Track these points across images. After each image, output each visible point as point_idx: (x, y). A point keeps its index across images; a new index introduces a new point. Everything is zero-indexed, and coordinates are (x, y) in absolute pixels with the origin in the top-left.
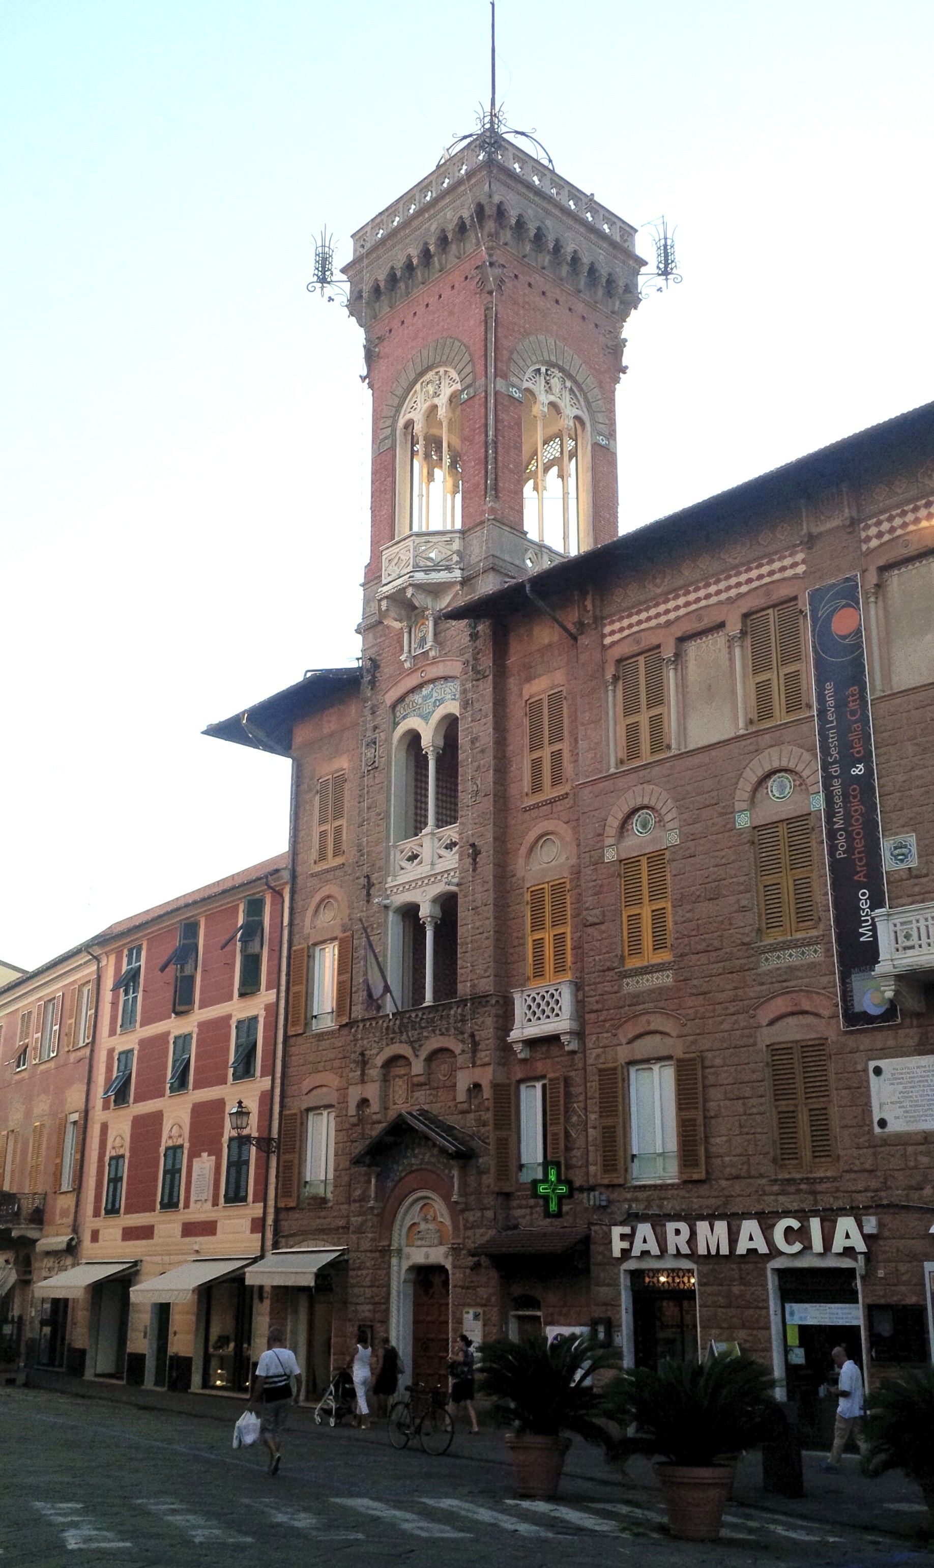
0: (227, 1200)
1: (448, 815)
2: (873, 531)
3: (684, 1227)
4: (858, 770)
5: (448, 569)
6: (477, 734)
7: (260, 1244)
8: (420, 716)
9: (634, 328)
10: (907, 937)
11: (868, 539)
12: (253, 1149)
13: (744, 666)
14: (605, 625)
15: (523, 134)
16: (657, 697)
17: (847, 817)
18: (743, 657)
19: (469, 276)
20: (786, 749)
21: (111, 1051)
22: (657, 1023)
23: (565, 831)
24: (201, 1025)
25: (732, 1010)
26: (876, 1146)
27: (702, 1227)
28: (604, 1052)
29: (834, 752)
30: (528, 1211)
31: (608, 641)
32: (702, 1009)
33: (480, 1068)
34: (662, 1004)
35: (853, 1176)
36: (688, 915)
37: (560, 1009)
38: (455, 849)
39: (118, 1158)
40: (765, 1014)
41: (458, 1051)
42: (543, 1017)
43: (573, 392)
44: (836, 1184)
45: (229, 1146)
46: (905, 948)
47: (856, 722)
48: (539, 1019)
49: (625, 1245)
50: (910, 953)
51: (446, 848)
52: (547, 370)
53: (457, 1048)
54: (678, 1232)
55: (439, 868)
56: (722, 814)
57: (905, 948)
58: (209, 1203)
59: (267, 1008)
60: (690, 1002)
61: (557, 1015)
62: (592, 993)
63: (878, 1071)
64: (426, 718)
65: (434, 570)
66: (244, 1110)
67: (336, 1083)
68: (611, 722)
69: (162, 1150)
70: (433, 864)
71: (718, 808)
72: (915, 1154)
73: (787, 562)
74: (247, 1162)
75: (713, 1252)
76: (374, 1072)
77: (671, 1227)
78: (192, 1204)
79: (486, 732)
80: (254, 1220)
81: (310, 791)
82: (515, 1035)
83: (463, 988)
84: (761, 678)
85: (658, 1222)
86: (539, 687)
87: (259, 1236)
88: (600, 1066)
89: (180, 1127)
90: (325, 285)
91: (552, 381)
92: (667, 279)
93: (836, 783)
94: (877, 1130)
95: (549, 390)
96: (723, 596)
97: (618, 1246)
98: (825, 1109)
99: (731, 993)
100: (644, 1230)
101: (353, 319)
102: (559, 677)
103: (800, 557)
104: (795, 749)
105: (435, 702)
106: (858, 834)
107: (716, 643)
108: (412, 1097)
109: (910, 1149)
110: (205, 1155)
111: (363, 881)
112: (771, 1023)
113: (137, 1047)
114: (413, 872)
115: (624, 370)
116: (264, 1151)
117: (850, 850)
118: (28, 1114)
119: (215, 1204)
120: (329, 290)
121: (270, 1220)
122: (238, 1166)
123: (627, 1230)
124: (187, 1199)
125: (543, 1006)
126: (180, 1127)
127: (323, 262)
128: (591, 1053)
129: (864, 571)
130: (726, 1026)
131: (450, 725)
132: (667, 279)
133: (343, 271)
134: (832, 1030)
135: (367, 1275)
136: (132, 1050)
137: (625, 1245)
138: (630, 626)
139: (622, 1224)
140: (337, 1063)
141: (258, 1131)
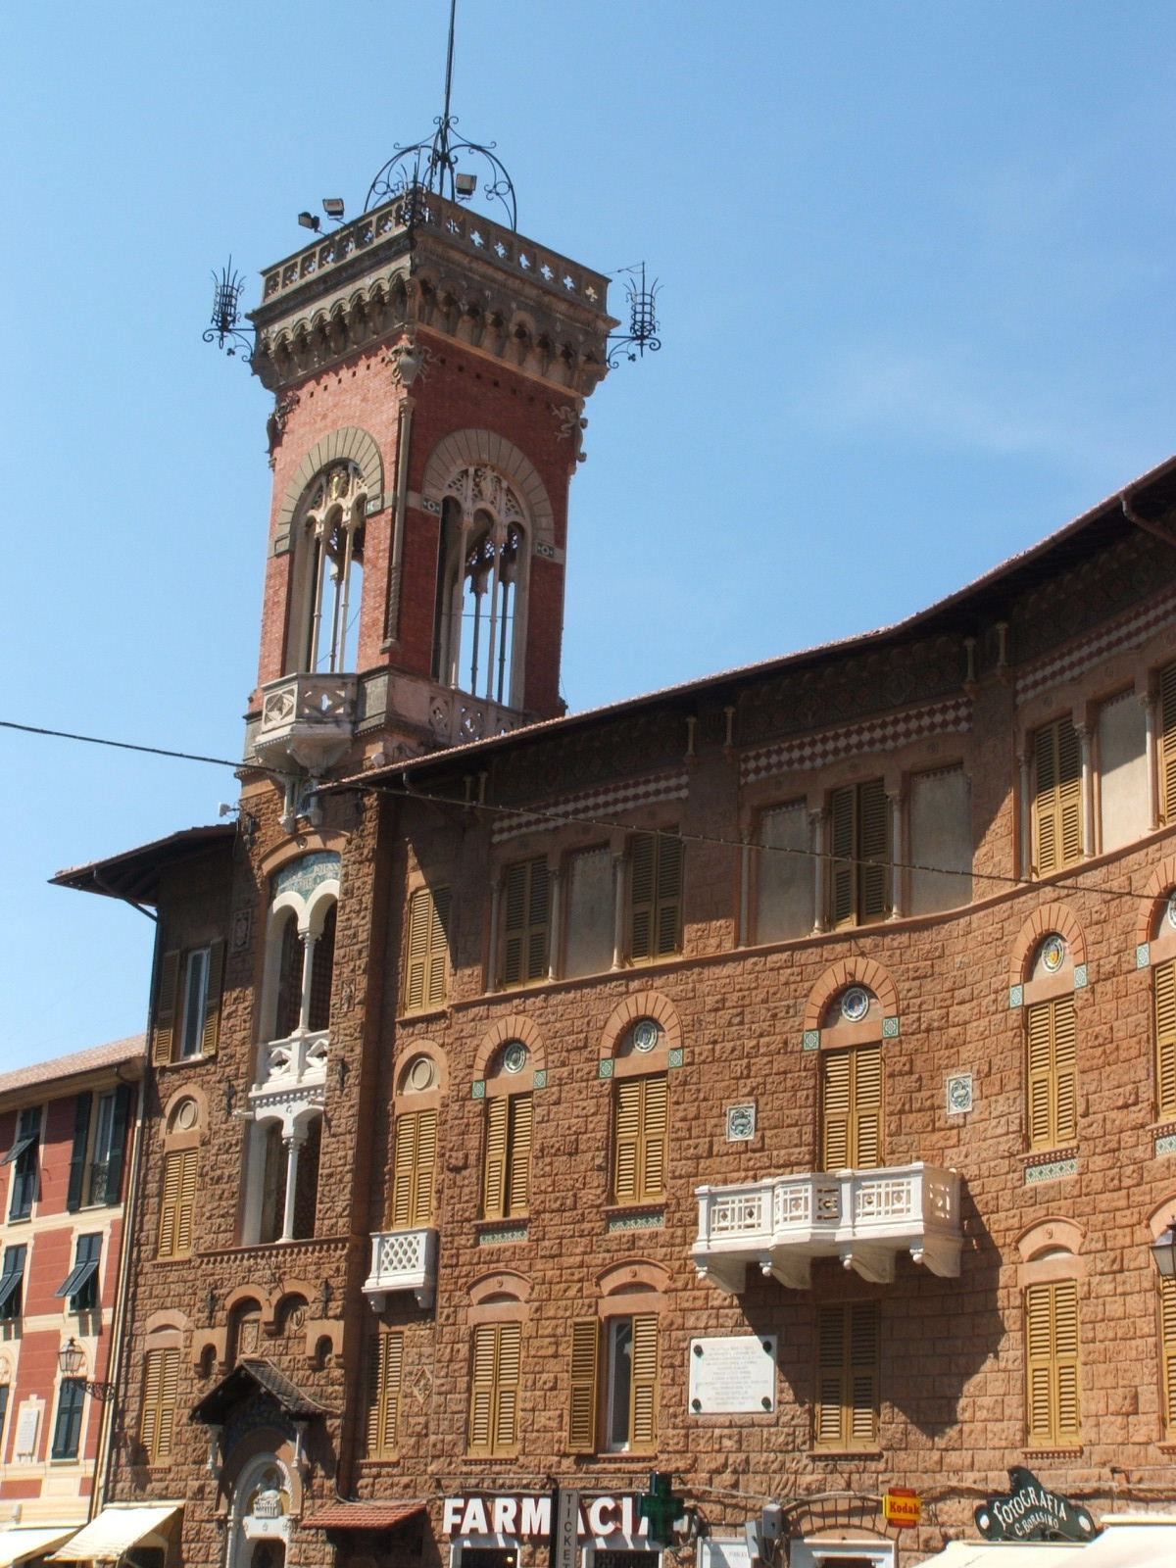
0: (56, 1455)
1: (318, 1021)
2: (752, 765)
3: (511, 1503)
6: (356, 928)
7: (88, 1510)
8: (299, 891)
11: (747, 773)
12: (88, 1398)
13: (625, 893)
14: (494, 820)
15: (479, 148)
16: (541, 916)
18: (625, 882)
19: (387, 359)
20: (652, 994)
22: (510, 1285)
23: (439, 1054)
24: (38, 1237)
27: (528, 1504)
28: (455, 1312)
30: (371, 1480)
33: (332, 1321)
36: (548, 1168)
37: (417, 1259)
38: (326, 1059)
40: (610, 1282)
41: (310, 1299)
42: (399, 1267)
43: (513, 494)
45: (61, 1389)
48: (395, 1268)
49: (457, 1519)
50: (725, 1234)
51: (318, 1056)
52: (476, 471)
53: (311, 1294)
54: (505, 1509)
56: (588, 1060)
58: (35, 1458)
59: (113, 1224)
60: (539, 1265)
61: (414, 1266)
62: (449, 1245)
63: (699, 1351)
66: (77, 1349)
67: (184, 1323)
68: (493, 936)
71: (585, 1054)
72: (721, 1437)
73: (673, 782)
74: (80, 1410)
75: (535, 1532)
77: (500, 1503)
78: (15, 1458)
79: (363, 925)
80: (84, 1480)
82: (371, 1285)
84: (641, 908)
85: (487, 1498)
87: (87, 1499)
89: (7, 1361)
90: (225, 334)
91: (483, 484)
92: (642, 345)
94: (692, 1410)
95: (478, 494)
96: (611, 810)
97: (449, 1520)
98: (838, 1380)
99: (578, 1259)
100: (475, 1505)
101: (257, 378)
103: (684, 779)
105: (315, 879)
107: (601, 861)
108: (261, 1346)
109: (717, 1432)
110: (33, 1397)
113: (31, 1244)
115: (583, 458)
116: (99, 1399)
119: (42, 1458)
120: (230, 340)
121: (101, 1482)
122: (70, 1413)
123: (460, 1503)
125: (401, 1255)
126: (7, 1361)
127: (226, 300)
128: (441, 1313)
131: (328, 911)
132: (642, 345)
133: (248, 317)
135: (200, 1549)
137: (457, 1519)
139: (456, 1496)
141: (96, 1372)
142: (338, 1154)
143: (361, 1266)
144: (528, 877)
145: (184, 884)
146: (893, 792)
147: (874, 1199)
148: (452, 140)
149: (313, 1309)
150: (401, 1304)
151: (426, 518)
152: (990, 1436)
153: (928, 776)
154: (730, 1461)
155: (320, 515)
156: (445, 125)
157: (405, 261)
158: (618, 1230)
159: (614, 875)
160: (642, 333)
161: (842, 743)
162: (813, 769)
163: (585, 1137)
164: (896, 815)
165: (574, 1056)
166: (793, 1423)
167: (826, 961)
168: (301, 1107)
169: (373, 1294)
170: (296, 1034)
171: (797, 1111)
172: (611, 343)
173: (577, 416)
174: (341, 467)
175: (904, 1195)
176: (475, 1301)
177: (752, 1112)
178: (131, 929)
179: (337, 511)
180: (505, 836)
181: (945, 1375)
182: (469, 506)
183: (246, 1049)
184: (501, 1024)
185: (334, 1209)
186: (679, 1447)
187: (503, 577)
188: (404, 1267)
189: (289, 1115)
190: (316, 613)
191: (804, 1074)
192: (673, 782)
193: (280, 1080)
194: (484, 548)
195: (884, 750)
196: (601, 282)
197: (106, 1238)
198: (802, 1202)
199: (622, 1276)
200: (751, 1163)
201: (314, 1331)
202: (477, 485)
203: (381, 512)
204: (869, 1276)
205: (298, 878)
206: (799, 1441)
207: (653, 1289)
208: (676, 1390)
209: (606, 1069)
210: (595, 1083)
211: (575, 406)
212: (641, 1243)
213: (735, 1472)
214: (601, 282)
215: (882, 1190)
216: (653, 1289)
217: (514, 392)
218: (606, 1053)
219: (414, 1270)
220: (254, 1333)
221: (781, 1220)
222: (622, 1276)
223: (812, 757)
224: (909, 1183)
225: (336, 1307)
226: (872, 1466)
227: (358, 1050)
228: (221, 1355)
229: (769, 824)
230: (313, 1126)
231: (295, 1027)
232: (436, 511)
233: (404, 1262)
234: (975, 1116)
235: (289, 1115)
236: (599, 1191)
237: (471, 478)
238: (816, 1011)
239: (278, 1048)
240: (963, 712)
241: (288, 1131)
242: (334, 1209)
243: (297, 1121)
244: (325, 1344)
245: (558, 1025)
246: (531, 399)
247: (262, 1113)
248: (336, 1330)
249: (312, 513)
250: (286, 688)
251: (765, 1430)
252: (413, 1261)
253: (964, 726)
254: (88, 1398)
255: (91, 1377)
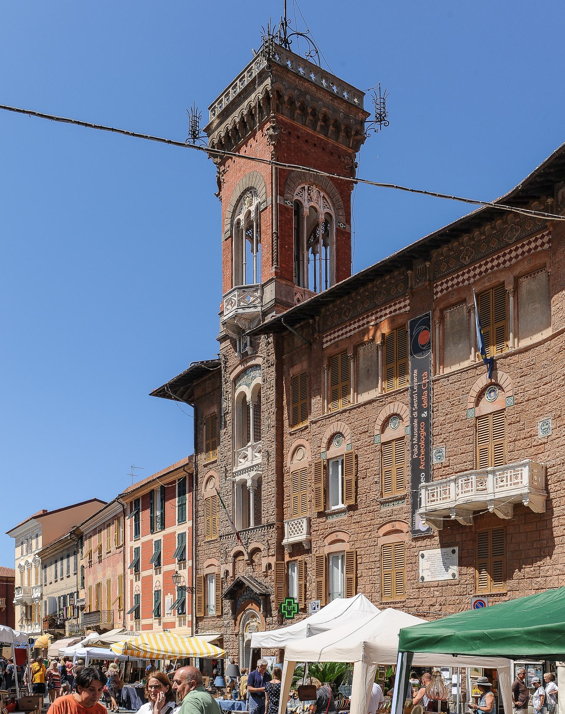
2: (439, 289)
4: (424, 415)
5: (255, 307)
9: (362, 157)
10: (433, 496)
11: (437, 293)
12: (187, 593)
15: (301, 35)
17: (419, 438)
18: (382, 355)
20: (396, 403)
21: (131, 548)
22: (341, 536)
25: (369, 529)
26: (419, 588)
29: (415, 405)
31: (325, 346)
32: (357, 529)
34: (342, 527)
35: (410, 600)
39: (137, 596)
42: (299, 532)
44: (403, 604)
46: (432, 501)
47: (425, 390)
50: (433, 503)
52: (308, 187)
55: (255, 463)
57: (432, 501)
58: (172, 615)
62: (315, 522)
63: (423, 556)
64: (248, 385)
65: (248, 307)
69: (153, 592)
70: (252, 460)
73: (402, 304)
76: (230, 559)
78: (166, 615)
81: (202, 423)
82: (285, 542)
83: (264, 521)
86: (296, 370)
88: (317, 555)
93: (416, 421)
95: (310, 200)
102: (305, 365)
103: (408, 302)
104: (401, 404)
106: (423, 446)
110: (169, 594)
111: (223, 469)
112: (385, 535)
113: (162, 539)
114: (243, 464)
117: (419, 454)
118: (104, 575)
124: (164, 613)
129: (434, 311)
130: (366, 537)
134: (406, 538)
136: (160, 540)
138: (335, 338)
140: (217, 554)
142: (269, 490)
143: (281, 535)
144: (340, 361)
145: (197, 386)
146: (509, 287)
147: (505, 479)
148: (289, 32)
149: (264, 553)
150: (298, 548)
151: (287, 209)
152: (560, 581)
153: (527, 277)
154: (438, 601)
155: (242, 217)
156: (284, 24)
157: (268, 81)
158: (385, 509)
159: (377, 353)
160: (381, 118)
161: (483, 268)
162: (469, 284)
163: (369, 470)
164: (511, 299)
165: (363, 436)
166: (466, 583)
167: (478, 375)
168: (253, 473)
169: (286, 545)
170: (249, 444)
171: (465, 446)
172: (366, 125)
173: (352, 162)
174: (250, 190)
175: (519, 476)
176: (327, 544)
177: (444, 449)
178: (183, 413)
179: (249, 212)
180: (329, 343)
181: (538, 557)
182: (306, 205)
183: (230, 453)
184: (332, 426)
185: (269, 512)
186: (415, 597)
187: (325, 245)
188: (298, 533)
189: (248, 477)
190: (244, 262)
191: (468, 429)
192: (402, 304)
193: (243, 464)
194: (316, 233)
195: (505, 267)
196: (360, 95)
197: (187, 534)
198: (470, 484)
199: (388, 528)
200: (444, 472)
201: (264, 562)
202: (309, 195)
203: (266, 208)
204: (501, 516)
205: (245, 379)
206: (469, 590)
207: (402, 532)
208: (413, 573)
209: (377, 439)
210: (373, 446)
211: (352, 157)
212: (396, 513)
213: (440, 605)
214: (360, 95)
215: (509, 475)
216: (402, 532)
217: (323, 149)
218: (377, 432)
219: (302, 534)
220: (243, 565)
221: (460, 493)
222: (388, 528)
223: (469, 279)
224: (522, 470)
225: (272, 551)
226: (504, 598)
227: (274, 446)
228: (231, 574)
229: (447, 313)
230: (258, 482)
231: (249, 441)
232: (291, 206)
233: (298, 531)
234: (554, 437)
235: (248, 477)
236: (376, 493)
237: (306, 191)
238: (473, 400)
239: (242, 451)
240: (546, 239)
241: (249, 483)
242: (269, 512)
243: (253, 479)
244: (269, 566)
245: (356, 423)
246: (332, 153)
247: (238, 478)
248: (273, 560)
249: (238, 217)
250: (232, 294)
251: (453, 587)
252: (301, 530)
253: (546, 246)
254: (187, 593)
255: (187, 586)
